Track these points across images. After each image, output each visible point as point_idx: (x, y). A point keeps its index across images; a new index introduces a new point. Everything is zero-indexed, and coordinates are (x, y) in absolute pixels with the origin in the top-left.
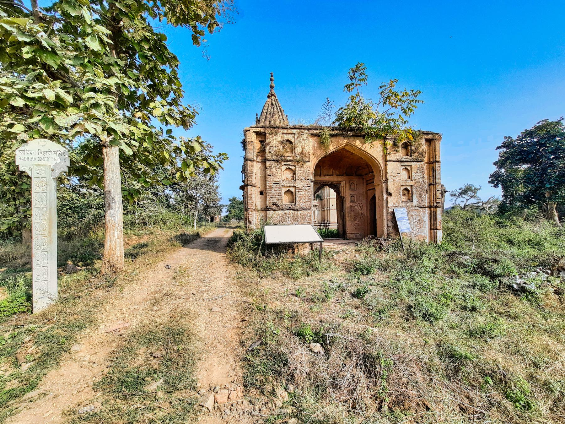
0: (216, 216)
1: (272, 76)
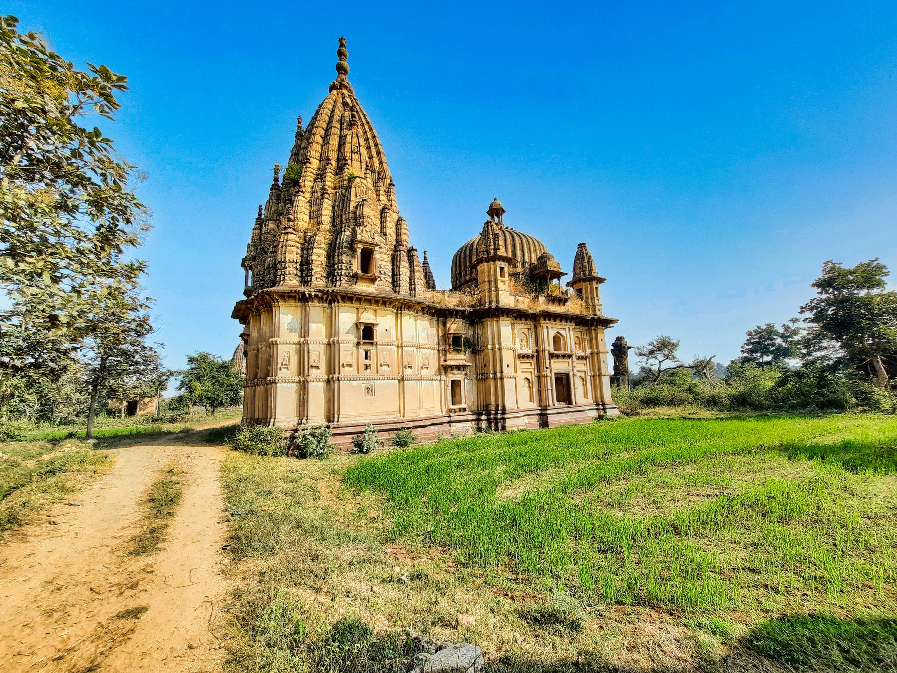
0: (146, 400)
1: (342, 45)
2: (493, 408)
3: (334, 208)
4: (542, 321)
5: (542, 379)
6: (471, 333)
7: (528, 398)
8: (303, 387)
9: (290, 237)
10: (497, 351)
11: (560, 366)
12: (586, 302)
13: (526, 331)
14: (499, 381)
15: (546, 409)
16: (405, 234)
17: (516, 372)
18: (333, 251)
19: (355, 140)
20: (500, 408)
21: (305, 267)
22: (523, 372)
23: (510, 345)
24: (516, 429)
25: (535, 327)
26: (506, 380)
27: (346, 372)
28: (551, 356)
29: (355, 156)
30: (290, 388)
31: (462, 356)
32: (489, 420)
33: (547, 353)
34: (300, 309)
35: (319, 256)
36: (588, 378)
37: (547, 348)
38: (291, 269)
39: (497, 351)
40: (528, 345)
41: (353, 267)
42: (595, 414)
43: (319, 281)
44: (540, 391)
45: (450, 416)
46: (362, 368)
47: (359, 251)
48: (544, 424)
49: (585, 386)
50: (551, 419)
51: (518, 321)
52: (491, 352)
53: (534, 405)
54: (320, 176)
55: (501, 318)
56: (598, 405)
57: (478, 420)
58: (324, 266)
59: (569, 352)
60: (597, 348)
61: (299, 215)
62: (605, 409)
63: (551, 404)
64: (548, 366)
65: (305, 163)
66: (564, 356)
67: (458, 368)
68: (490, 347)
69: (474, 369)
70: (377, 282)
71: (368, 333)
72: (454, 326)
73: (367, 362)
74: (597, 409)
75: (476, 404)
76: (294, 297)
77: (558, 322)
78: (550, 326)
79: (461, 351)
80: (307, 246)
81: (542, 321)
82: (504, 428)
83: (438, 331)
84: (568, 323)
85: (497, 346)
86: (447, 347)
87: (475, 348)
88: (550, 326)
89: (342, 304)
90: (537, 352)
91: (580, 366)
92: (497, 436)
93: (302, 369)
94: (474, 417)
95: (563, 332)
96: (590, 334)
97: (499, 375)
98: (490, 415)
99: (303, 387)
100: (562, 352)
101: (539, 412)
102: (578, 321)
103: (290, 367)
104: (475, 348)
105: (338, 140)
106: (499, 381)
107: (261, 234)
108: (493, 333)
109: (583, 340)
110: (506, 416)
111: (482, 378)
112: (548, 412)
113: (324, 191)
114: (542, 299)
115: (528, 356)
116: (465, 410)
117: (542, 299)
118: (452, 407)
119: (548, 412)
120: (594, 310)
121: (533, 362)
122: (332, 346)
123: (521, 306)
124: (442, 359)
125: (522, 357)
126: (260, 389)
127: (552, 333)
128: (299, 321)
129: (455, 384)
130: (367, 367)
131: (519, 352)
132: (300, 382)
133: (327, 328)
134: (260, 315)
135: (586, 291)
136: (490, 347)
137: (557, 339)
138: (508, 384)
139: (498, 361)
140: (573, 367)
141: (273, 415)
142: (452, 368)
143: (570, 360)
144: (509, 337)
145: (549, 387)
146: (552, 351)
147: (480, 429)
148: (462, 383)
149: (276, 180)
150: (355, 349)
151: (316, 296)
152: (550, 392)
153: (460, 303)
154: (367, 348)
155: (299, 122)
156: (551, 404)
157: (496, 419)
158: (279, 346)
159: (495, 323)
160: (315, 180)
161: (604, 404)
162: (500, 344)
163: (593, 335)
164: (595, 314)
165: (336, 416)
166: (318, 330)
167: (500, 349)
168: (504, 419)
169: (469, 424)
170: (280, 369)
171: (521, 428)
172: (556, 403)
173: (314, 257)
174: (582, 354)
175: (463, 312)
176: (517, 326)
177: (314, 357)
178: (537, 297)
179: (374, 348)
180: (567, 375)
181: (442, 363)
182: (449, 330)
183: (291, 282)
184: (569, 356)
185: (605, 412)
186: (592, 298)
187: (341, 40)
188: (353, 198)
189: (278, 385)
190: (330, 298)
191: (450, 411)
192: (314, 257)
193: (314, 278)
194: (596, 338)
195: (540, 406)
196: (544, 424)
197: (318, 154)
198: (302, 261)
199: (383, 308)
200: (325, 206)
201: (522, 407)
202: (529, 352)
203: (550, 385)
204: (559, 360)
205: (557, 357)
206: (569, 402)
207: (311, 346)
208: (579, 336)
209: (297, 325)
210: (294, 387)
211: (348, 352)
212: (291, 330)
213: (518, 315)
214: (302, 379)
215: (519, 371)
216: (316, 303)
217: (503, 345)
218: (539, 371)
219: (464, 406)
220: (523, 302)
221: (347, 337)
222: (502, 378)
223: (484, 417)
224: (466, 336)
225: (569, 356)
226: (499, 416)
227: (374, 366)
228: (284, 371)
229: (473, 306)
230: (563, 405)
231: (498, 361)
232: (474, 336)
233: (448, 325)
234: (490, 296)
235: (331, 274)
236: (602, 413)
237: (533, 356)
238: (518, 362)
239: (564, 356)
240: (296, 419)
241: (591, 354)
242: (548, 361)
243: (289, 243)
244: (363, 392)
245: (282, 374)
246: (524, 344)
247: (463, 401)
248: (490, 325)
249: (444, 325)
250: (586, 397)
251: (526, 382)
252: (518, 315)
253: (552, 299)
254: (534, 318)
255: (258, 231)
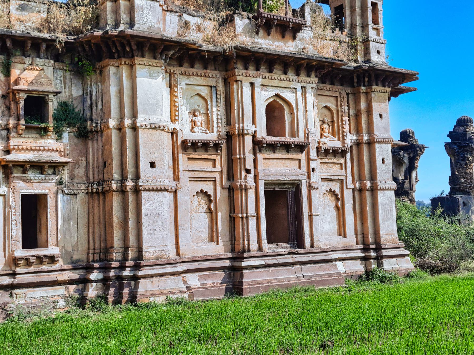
2: (117, 255)
4: (239, 71)
5: (238, 195)
6: (76, 92)
7: (206, 234)
10: (129, 133)
11: (278, 168)
12: (352, 35)
13: (205, 91)
14: (131, 197)
15: (242, 258)
17: (176, 178)
20: (131, 255)
22: (192, 179)
23: (164, 118)
24: (160, 300)
25: (227, 83)
26: (144, 195)
28: (258, 145)
31: (50, 142)
32: (105, 281)
33: (248, 140)
36: (348, 195)
37: (249, 127)
39: (129, 133)
40: (209, 122)
42: (358, 267)
44: (232, 220)
45: (13, 275)
48: (235, 288)
49: (340, 211)
50: (249, 278)
51: (186, 69)
52: (114, 136)
53: (219, 249)
55: (138, 60)
56: (366, 249)
57: (84, 282)
59: (301, 139)
60: (370, 131)
62: (379, 258)
63: (254, 246)
64: (250, 166)
66: (287, 147)
67: (39, 167)
68: (112, 123)
69: (81, 171)
72: (30, 75)
74: (365, 259)
75: (83, 247)
77: (277, 73)
78: (258, 82)
79: (46, 130)
81: (239, 71)
82: (133, 298)
84: (303, 77)
85: (128, 122)
86: (12, 122)
87: (83, 125)
88: (258, 82)
90: (229, 137)
91: (323, 169)
92: (113, 315)
94: (76, 275)
95: (289, 96)
96: (357, 102)
97: (130, 184)
98: (110, 269)
100: (287, 138)
101: (227, 263)
102: (327, 73)
104: (83, 125)
106: (131, 197)
108: (120, 93)
109: (340, 114)
110: (141, 273)
111: (98, 193)
112: (245, 263)
114: (241, 23)
115: (205, 146)
116: (52, 259)
117: (241, 23)
118: (20, 253)
119: (245, 263)
120: (367, 52)
121: (220, 159)
123: (193, 36)
125: (191, 146)
127: (264, 97)
129: (33, 208)
131: (186, 134)
135: (353, 10)
136: (112, 123)
137: (274, 112)
138: (155, 206)
139: (129, 154)
140: (310, 170)
142: (23, 166)
143: (303, 157)
144: (157, 101)
145: (252, 211)
146: (262, 134)
147: (82, 302)
148: (50, 202)
152: (252, 222)
153: (47, 24)
156: (254, 246)
157: (119, 278)
159: (125, 72)
161: (378, 249)
162: (134, 116)
163: (363, 105)
164: (368, 61)
167: (134, 128)
168: (136, 278)
169: (61, 290)
171: (173, 297)
172: (265, 245)
174: (337, 144)
175: (50, 43)
176: (182, 83)
178: (230, 20)
180: (296, 186)
182: (17, 82)
184: (301, 148)
185: (380, 265)
186: (364, 27)
191: (15, 261)
194: (369, 111)
195: (233, 250)
196: (235, 288)
201: (188, 251)
202: (211, 137)
203: (254, 206)
204: (277, 155)
205: (272, 147)
206: (297, 240)
208: (332, 106)
213: (179, 55)
215: (184, 176)
217: (140, 120)
218: (231, 175)
219: (52, 250)
220: (199, 29)
222: (137, 191)
223: (94, 276)
224: (63, 97)
225: (301, 148)
226: (126, 273)
229: (76, 32)
230: (284, 248)
231: (129, 154)
232: (83, 98)
233: (15, 72)
234: (116, 11)
236: (374, 266)
237: (217, 146)
238: (182, 158)
239: (287, 147)
241: (358, 144)
242: (249, 158)
246: (200, 119)
247: (52, 239)
248: (116, 74)
250: (342, 232)
251: (203, 201)
252: (179, 55)
253: (266, 25)
254: (225, 64)
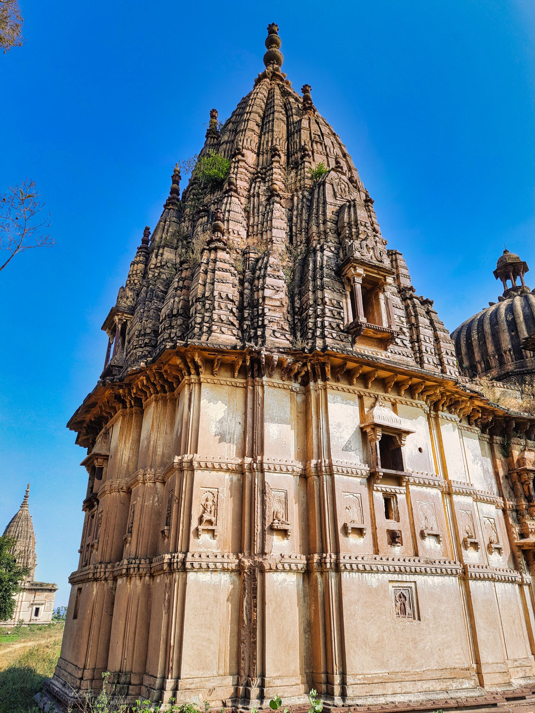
3: (290, 220)
8: (250, 583)
9: (221, 254)
16: (405, 276)
18: (299, 283)
19: (314, 127)
21: (250, 311)
27: (354, 547)
29: (317, 147)
30: (216, 587)
34: (240, 392)
35: (275, 293)
38: (223, 312)
41: (344, 314)
43: (277, 339)
46: (383, 539)
47: (359, 280)
54: (261, 174)
58: (285, 310)
61: (232, 225)
65: (234, 156)
70: (391, 347)
71: (386, 450)
73: (392, 525)
76: (230, 367)
80: (252, 276)
83: (495, 466)
89: (331, 383)
93: (248, 535)
99: (250, 583)
103: (219, 528)
105: (285, 127)
107: (145, 274)
113: (272, 194)
122: (314, 481)
124: (516, 530)
126: (131, 588)
128: (240, 419)
130: (394, 538)
132: (239, 570)
133: (297, 436)
134: (141, 413)
141: (173, 665)
149: (174, 191)
150: (365, 490)
151: (280, 363)
154: (390, 488)
155: (213, 116)
158: (198, 474)
160: (253, 181)
165: (337, 679)
166: (280, 436)
170: (197, 535)
173: (268, 293)
177: (274, 506)
179: (403, 489)
181: (518, 541)
183: (226, 337)
187: (271, 30)
188: (330, 199)
189: (191, 576)
190: (311, 370)
192: (268, 293)
193: (268, 332)
197: (254, 146)
198: (242, 302)
199: (409, 400)
200: (276, 214)
207: (268, 476)
209: (235, 428)
210: (226, 582)
211: (352, 497)
212: (222, 439)
214: (247, 562)
216: (276, 379)
221: (348, 457)
227: (406, 536)
228: (205, 537)
233: (516, 454)
235: (299, 320)
240: (230, 680)
243: (219, 264)
244: (391, 605)
245: (203, 546)
249: (507, 452)
255: (141, 266)
